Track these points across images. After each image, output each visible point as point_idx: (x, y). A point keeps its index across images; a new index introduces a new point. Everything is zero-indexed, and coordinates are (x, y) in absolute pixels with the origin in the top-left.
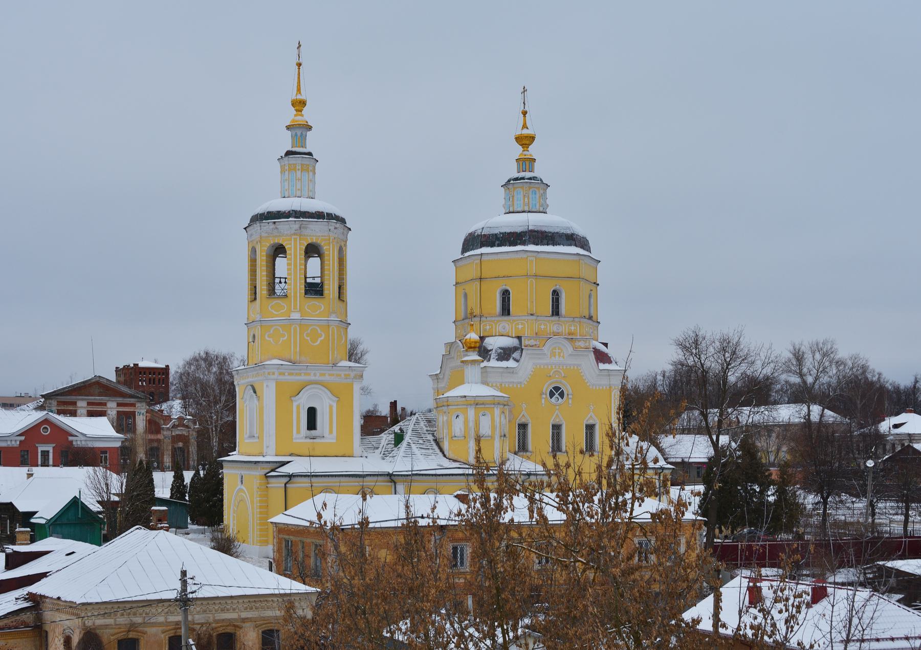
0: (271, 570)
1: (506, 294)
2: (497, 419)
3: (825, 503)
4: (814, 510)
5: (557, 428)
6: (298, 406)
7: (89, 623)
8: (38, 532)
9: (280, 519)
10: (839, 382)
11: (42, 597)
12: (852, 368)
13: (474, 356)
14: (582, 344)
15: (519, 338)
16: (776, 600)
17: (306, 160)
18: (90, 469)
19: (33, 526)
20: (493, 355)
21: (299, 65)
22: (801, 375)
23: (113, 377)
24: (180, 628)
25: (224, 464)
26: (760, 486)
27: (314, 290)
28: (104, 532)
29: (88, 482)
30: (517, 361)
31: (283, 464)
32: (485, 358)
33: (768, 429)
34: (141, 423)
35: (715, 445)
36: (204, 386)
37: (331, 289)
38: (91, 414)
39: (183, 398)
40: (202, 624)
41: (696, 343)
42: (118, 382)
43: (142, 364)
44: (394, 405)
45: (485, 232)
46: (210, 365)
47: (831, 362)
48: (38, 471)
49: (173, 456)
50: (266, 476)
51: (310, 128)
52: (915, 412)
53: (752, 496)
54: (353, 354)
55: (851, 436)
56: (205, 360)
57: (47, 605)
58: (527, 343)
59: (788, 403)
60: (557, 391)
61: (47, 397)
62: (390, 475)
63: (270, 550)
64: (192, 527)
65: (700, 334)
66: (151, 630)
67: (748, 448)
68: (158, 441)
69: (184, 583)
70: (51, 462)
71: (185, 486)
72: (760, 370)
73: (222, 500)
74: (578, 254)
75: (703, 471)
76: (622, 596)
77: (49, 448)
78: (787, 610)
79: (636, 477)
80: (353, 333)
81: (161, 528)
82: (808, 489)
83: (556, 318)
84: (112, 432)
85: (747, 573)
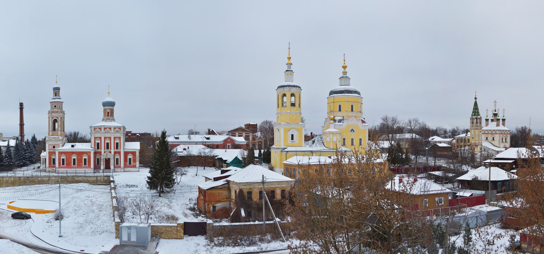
0: (283, 175)
1: (340, 106)
2: (338, 137)
3: (416, 158)
4: (414, 159)
5: (352, 139)
6: (289, 134)
7: (241, 187)
8: (228, 165)
9: (285, 162)
10: (419, 128)
11: (230, 181)
12: (422, 125)
13: (332, 122)
14: (358, 118)
15: (343, 117)
16: (407, 184)
17: (291, 72)
18: (240, 149)
19: (227, 163)
20: (337, 121)
21: (289, 48)
22: (411, 126)
23: (244, 127)
24: (262, 189)
25: (271, 149)
26: (401, 154)
27: (293, 105)
28: (243, 165)
29: (239, 153)
30: (343, 123)
31: (286, 148)
32: (335, 122)
33: (403, 140)
34: (251, 138)
35: (391, 144)
36: (266, 129)
37: (297, 105)
38: (239, 136)
39: (261, 132)
40: (267, 188)
41: (386, 118)
42: (245, 128)
43: (251, 123)
44: (312, 133)
45: (335, 90)
46: (267, 123)
47: (418, 124)
48: (227, 150)
49: (258, 146)
50: (281, 151)
51: (292, 64)
52: (437, 136)
53: (399, 156)
54: (302, 121)
55: (422, 142)
56: (266, 122)
57: (231, 183)
58: (345, 118)
59: (408, 133)
60: (352, 130)
61: (229, 132)
62: (311, 151)
63: (282, 170)
64: (263, 164)
65: (387, 117)
66: (255, 190)
67: (398, 145)
68: (255, 142)
69: (263, 178)
70: (230, 148)
71: (262, 154)
72: (401, 125)
73: (271, 157)
74: (358, 96)
75: (388, 150)
76: (372, 183)
77: (230, 144)
78: (410, 186)
79: (375, 154)
80: (302, 115)
81: (257, 165)
82: (412, 155)
83: (352, 112)
84: (244, 140)
85: (399, 175)
